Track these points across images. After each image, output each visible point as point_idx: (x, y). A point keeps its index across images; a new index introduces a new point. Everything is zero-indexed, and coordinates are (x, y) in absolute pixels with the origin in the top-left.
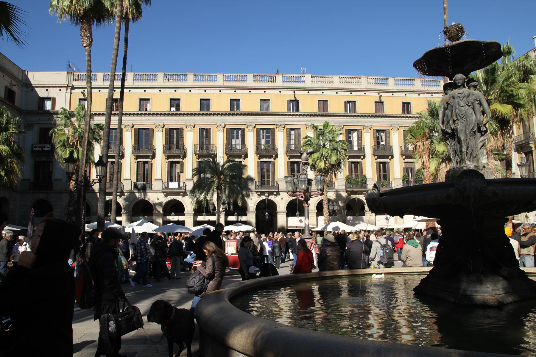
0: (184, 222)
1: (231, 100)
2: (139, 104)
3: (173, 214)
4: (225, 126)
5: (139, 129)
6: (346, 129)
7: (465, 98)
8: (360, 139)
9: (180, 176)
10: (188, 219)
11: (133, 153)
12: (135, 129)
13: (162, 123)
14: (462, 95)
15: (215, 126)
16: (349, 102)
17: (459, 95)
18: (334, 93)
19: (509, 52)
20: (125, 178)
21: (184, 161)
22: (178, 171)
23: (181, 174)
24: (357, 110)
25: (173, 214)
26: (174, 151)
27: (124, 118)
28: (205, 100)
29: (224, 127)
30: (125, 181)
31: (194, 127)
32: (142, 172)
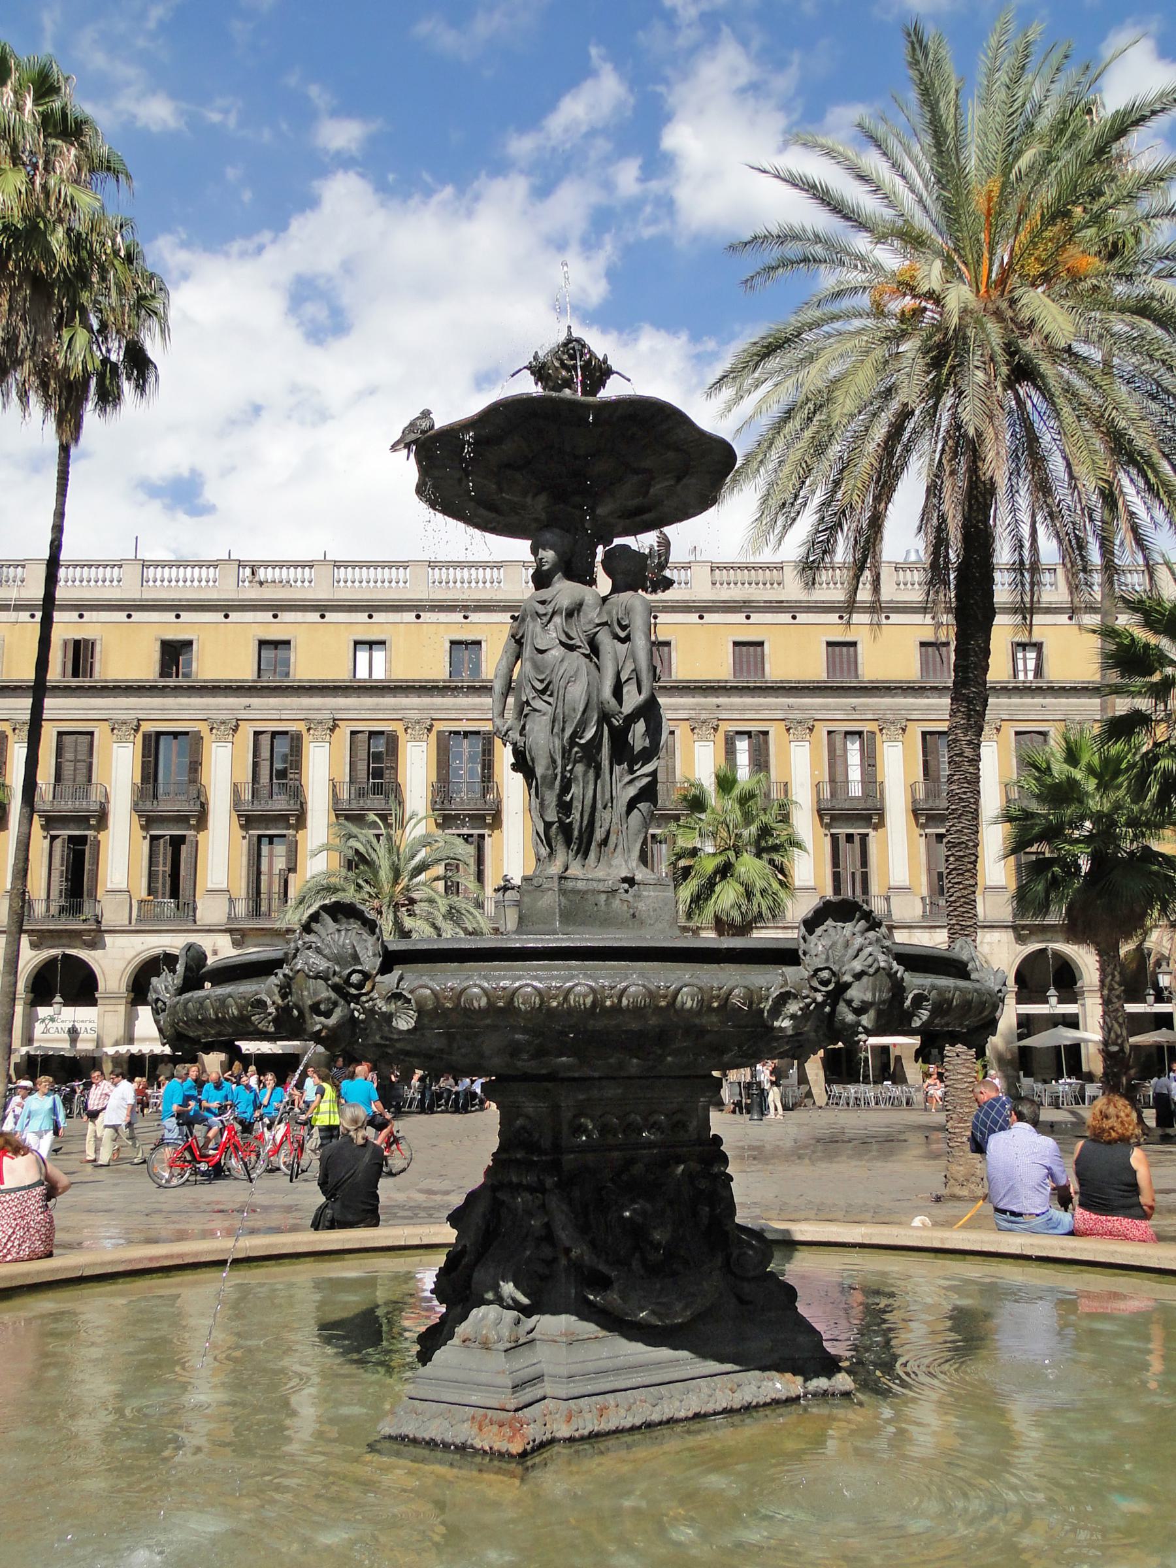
0: (1170, 1015)
1: (452, 643)
2: (447, 659)
3: (58, 999)
4: (138, 726)
5: (159, 734)
6: (439, 732)
7: (557, 620)
8: (870, 761)
9: (286, 882)
10: (1091, 1010)
11: (136, 808)
12: (147, 737)
13: (132, 716)
14: (549, 609)
15: (106, 726)
16: (1023, 646)
17: (541, 609)
18: (121, 616)
19: (394, 448)
20: (109, 886)
21: (100, 837)
22: (280, 864)
23: (291, 875)
24: (860, 672)
25: (58, 999)
26: (167, 805)
27: (48, 702)
28: (277, 644)
29: (136, 731)
30: (110, 896)
31: (235, 729)
32: (168, 869)
